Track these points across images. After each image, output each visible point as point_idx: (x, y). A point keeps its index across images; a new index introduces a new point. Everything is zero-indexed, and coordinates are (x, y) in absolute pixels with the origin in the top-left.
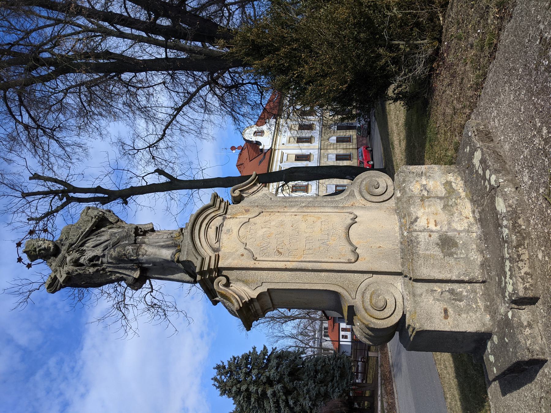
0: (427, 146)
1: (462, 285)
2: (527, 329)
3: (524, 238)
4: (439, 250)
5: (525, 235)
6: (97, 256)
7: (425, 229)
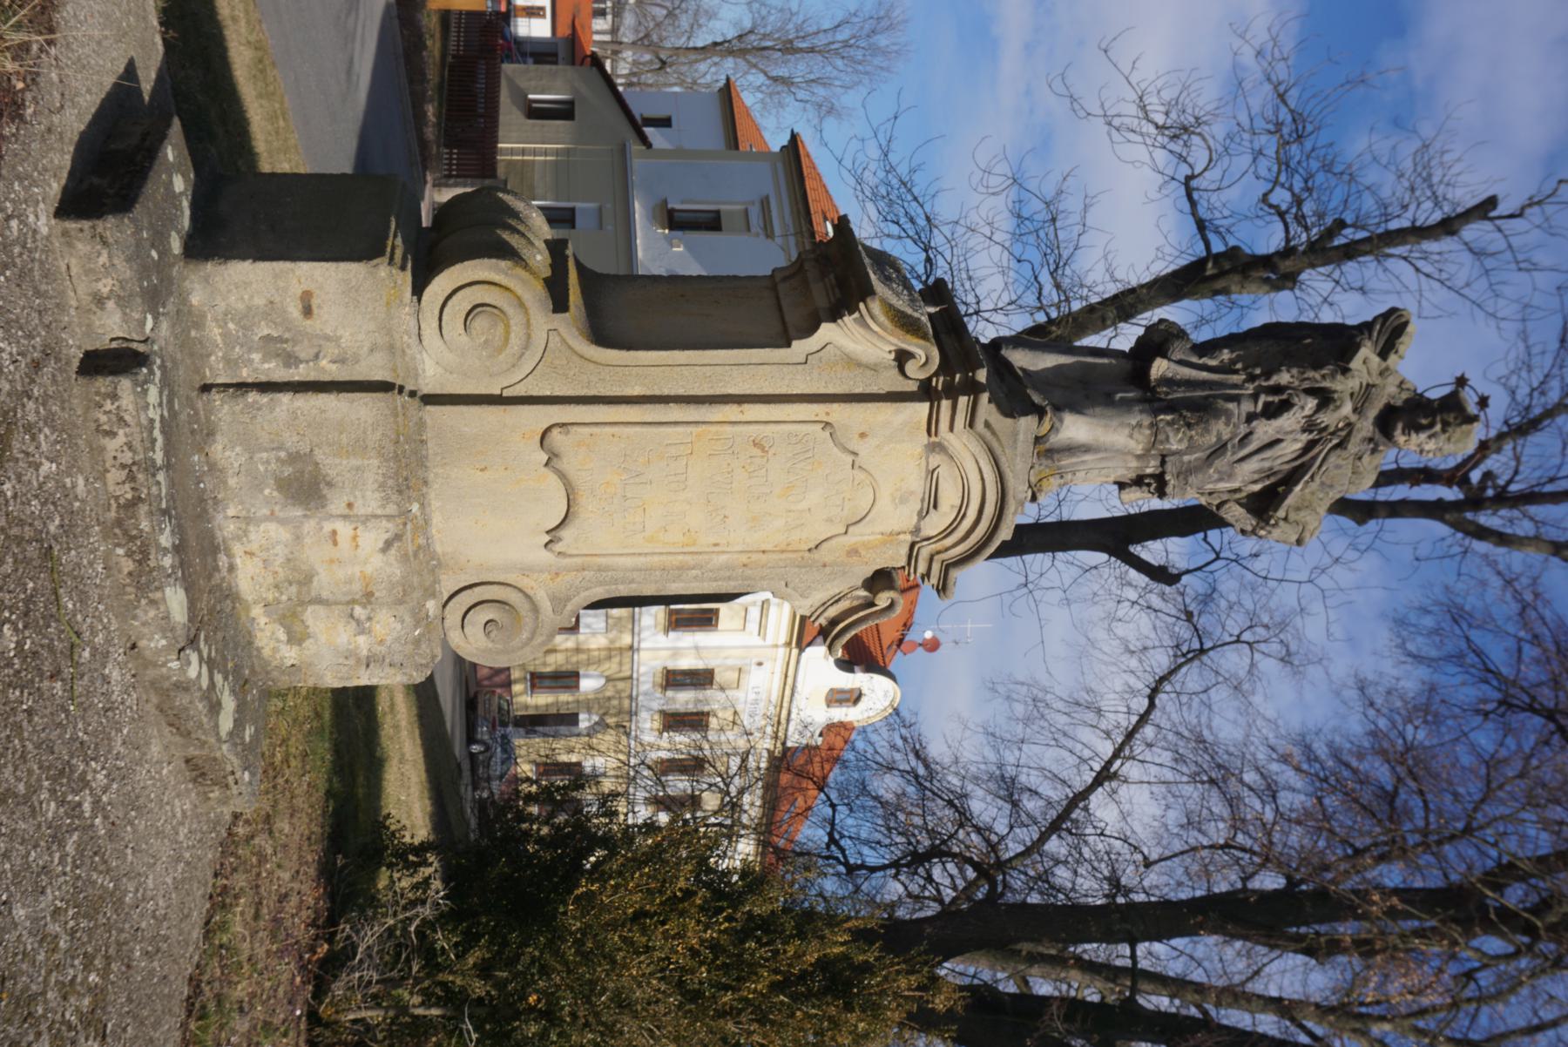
0: (327, 715)
1: (263, 378)
2: (105, 291)
3: (119, 522)
4: (325, 470)
5: (117, 531)
6: (1269, 418)
7: (364, 523)
